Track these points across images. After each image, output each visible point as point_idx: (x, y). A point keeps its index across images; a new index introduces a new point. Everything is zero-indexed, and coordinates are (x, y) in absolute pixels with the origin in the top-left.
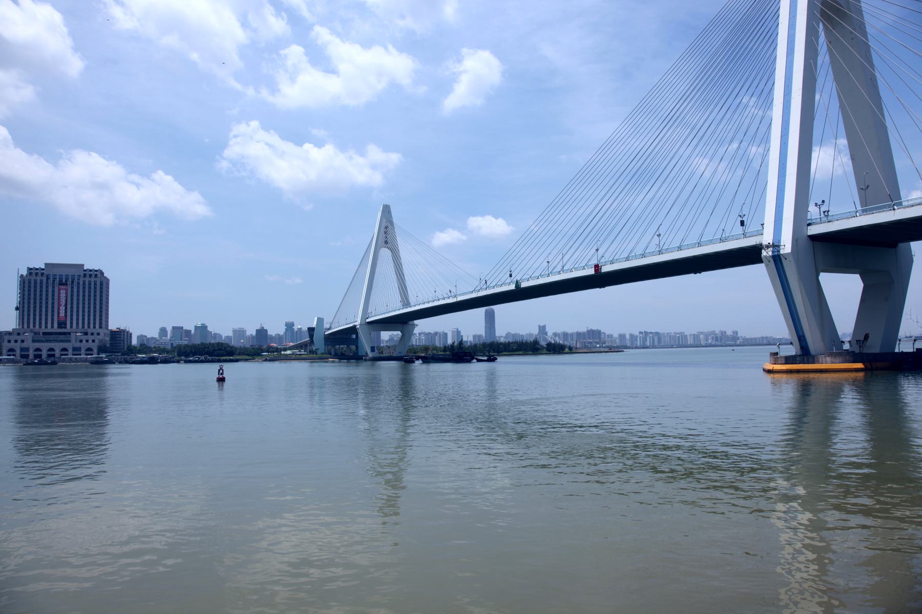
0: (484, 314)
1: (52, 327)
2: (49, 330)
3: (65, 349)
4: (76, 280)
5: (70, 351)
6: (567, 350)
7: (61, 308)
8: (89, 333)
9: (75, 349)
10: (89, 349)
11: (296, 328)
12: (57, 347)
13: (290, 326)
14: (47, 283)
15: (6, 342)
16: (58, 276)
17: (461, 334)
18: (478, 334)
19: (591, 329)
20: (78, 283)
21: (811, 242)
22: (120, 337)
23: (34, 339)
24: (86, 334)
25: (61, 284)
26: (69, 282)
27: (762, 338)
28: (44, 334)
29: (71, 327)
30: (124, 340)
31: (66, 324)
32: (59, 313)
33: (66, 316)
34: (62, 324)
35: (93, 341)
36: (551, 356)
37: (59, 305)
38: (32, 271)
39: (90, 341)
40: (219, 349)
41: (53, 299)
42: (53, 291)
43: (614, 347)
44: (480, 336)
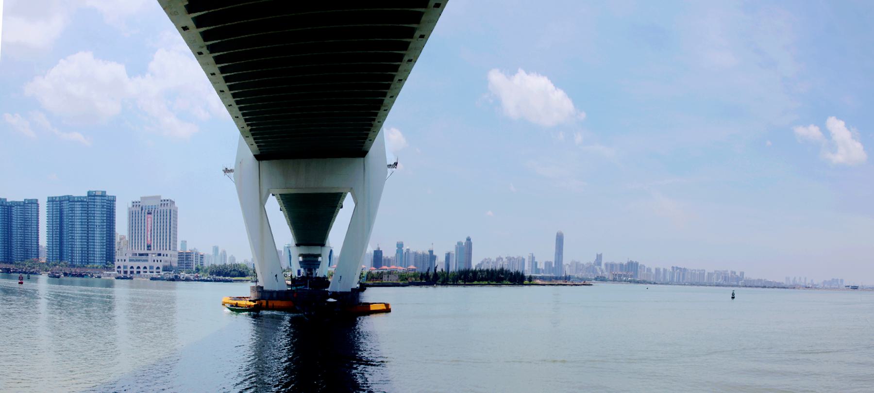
6: (526, 282)
11: (404, 249)
12: (142, 265)
14: (141, 213)
15: (117, 261)
17: (536, 261)
18: (549, 261)
21: (257, 162)
23: (131, 259)
24: (159, 255)
25: (149, 213)
26: (153, 212)
27: (759, 280)
34: (149, 247)
36: (455, 288)
37: (148, 231)
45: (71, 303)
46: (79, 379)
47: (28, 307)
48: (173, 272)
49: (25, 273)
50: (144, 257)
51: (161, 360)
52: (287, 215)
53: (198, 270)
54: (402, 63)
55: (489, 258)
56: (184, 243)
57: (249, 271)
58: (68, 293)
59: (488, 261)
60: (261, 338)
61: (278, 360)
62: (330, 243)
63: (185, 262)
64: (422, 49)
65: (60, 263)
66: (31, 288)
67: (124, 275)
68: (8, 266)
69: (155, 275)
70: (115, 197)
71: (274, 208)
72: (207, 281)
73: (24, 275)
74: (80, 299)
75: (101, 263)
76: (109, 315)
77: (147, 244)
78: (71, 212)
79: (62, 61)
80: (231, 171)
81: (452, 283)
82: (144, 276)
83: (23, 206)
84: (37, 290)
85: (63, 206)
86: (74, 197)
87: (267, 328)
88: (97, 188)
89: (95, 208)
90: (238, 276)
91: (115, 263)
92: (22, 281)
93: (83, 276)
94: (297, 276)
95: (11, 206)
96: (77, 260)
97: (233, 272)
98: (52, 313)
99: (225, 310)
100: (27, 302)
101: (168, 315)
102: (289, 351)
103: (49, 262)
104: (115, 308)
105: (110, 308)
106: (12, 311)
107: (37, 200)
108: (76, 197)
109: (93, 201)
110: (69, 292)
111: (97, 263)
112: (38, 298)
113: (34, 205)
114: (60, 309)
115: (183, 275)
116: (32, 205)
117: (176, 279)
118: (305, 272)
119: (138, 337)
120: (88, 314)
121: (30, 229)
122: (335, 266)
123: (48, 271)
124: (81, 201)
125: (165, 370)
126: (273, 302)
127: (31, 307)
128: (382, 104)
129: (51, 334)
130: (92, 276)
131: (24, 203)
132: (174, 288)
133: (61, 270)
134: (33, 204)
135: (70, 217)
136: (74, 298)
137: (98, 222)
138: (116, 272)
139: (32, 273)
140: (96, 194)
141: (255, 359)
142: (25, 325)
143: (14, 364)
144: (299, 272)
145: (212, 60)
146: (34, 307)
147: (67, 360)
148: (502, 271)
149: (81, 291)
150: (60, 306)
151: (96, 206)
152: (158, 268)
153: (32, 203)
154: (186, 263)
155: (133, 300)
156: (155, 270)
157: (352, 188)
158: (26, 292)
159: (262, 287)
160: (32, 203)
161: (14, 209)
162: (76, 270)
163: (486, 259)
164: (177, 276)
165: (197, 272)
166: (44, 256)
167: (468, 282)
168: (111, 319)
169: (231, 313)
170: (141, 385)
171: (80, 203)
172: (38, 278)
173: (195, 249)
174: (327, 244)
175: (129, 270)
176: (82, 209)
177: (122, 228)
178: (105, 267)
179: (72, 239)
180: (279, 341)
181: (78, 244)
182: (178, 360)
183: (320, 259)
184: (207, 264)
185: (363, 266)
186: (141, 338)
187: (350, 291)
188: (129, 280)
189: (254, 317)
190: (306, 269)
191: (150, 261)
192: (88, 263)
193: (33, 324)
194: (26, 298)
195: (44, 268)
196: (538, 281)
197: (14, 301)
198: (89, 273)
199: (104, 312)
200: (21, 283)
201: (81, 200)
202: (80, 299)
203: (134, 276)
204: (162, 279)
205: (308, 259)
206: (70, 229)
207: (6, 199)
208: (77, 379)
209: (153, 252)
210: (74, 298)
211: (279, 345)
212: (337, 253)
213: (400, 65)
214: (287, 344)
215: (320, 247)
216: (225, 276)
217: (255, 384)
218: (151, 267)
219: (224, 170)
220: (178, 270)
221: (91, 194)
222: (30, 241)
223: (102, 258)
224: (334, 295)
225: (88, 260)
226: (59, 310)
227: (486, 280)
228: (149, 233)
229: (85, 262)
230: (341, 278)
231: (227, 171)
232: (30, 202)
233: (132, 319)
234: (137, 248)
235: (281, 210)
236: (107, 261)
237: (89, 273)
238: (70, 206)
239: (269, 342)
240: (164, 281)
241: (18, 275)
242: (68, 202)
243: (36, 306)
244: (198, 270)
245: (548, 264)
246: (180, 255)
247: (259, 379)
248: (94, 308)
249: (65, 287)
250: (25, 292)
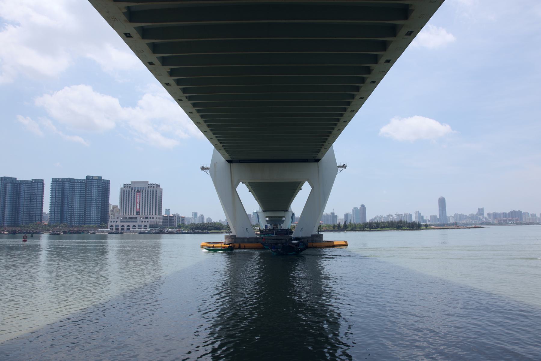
0: (438, 201)
1: (134, 214)
2: (132, 216)
3: (134, 226)
4: (145, 189)
5: (137, 227)
6: (422, 227)
7: (138, 204)
8: (149, 218)
9: (139, 226)
10: (145, 226)
12: (131, 224)
13: (195, 214)
14: (132, 191)
15: (110, 222)
16: (145, 188)
19: (514, 211)
20: (145, 191)
21: (229, 164)
24: (147, 218)
28: (130, 218)
29: (142, 214)
30: (175, 221)
31: (140, 213)
32: (136, 207)
33: (140, 209)
34: (138, 213)
35: (148, 222)
39: (146, 222)
40: (211, 226)
41: (134, 200)
42: (134, 196)
43: (448, 225)
45: (68, 252)
46: (73, 305)
47: (30, 258)
48: (158, 228)
49: (29, 233)
50: (133, 220)
51: (146, 285)
52: (255, 194)
54: (345, 112)
57: (224, 227)
58: (66, 245)
59: (381, 217)
60: (234, 266)
61: (250, 278)
62: (292, 209)
63: (169, 222)
65: (60, 225)
66: (34, 244)
67: (116, 231)
68: (14, 229)
70: (110, 180)
71: (243, 190)
73: (27, 235)
74: (76, 249)
76: (102, 258)
77: (136, 211)
78: (71, 189)
79: (66, 88)
80: (207, 168)
81: (359, 230)
83: (30, 184)
84: (39, 245)
85: (64, 185)
86: (75, 179)
87: (240, 260)
90: (214, 230)
91: (108, 223)
92: (26, 239)
93: (80, 233)
94: (264, 229)
95: (20, 184)
96: (76, 222)
97: (210, 227)
98: (52, 261)
99: (203, 250)
100: (28, 255)
101: (153, 255)
102: (259, 273)
103: (51, 224)
104: (107, 253)
105: (103, 253)
106: (14, 263)
107: (43, 180)
108: (76, 179)
110: (67, 244)
112: (39, 251)
113: (40, 183)
114: (58, 257)
116: (38, 183)
119: (126, 271)
120: (83, 259)
121: (36, 201)
122: (297, 222)
123: (50, 231)
124: (81, 183)
125: (151, 291)
127: (33, 257)
128: (331, 133)
129: (49, 276)
130: (88, 232)
131: (32, 181)
132: (159, 239)
133: (61, 230)
134: (40, 183)
135: (70, 193)
136: (71, 249)
137: (94, 196)
139: (36, 233)
140: (93, 178)
141: (230, 278)
142: (26, 272)
143: (13, 303)
144: (266, 227)
145: (191, 105)
146: (35, 257)
147: (62, 293)
148: (401, 222)
149: (78, 243)
150: (59, 255)
151: (93, 186)
153: (38, 182)
154: (169, 223)
155: (123, 247)
158: (29, 247)
159: (236, 236)
160: (38, 182)
161: (23, 186)
162: (74, 229)
165: (179, 228)
166: (47, 220)
167: (372, 229)
168: (103, 261)
169: (208, 252)
170: (128, 303)
171: (79, 184)
172: (40, 236)
173: (177, 214)
174: (289, 210)
175: (120, 228)
176: (81, 188)
177: (115, 199)
178: (99, 226)
179: (71, 208)
180: (251, 267)
181: (76, 211)
182: (162, 283)
185: (321, 222)
186: (129, 272)
187: (311, 236)
189: (228, 254)
190: (272, 225)
191: (138, 222)
192: (85, 224)
193: (33, 271)
194: (28, 252)
195: (46, 229)
197: (18, 255)
198: (86, 231)
199: (97, 257)
200: (25, 241)
201: (80, 181)
202: (76, 249)
203: (125, 231)
204: (149, 233)
205: (273, 219)
206: (70, 201)
207: (16, 178)
208: (70, 305)
209: (141, 216)
210: (71, 249)
211: (250, 269)
213: (345, 113)
214: (257, 268)
215: (283, 212)
216: (203, 230)
217: (230, 294)
218: (139, 226)
220: (164, 226)
221: (89, 178)
222: (35, 211)
224: (297, 239)
225: (85, 222)
226: (58, 258)
227: (388, 228)
229: (82, 223)
231: (203, 168)
232: (36, 181)
233: (123, 260)
235: (249, 191)
237: (86, 231)
238: (71, 185)
239: (241, 268)
240: (151, 234)
241: (23, 235)
242: (69, 182)
243: (37, 257)
244: (179, 227)
246: (165, 218)
247: (234, 291)
248: (89, 254)
249: (64, 241)
250: (28, 248)
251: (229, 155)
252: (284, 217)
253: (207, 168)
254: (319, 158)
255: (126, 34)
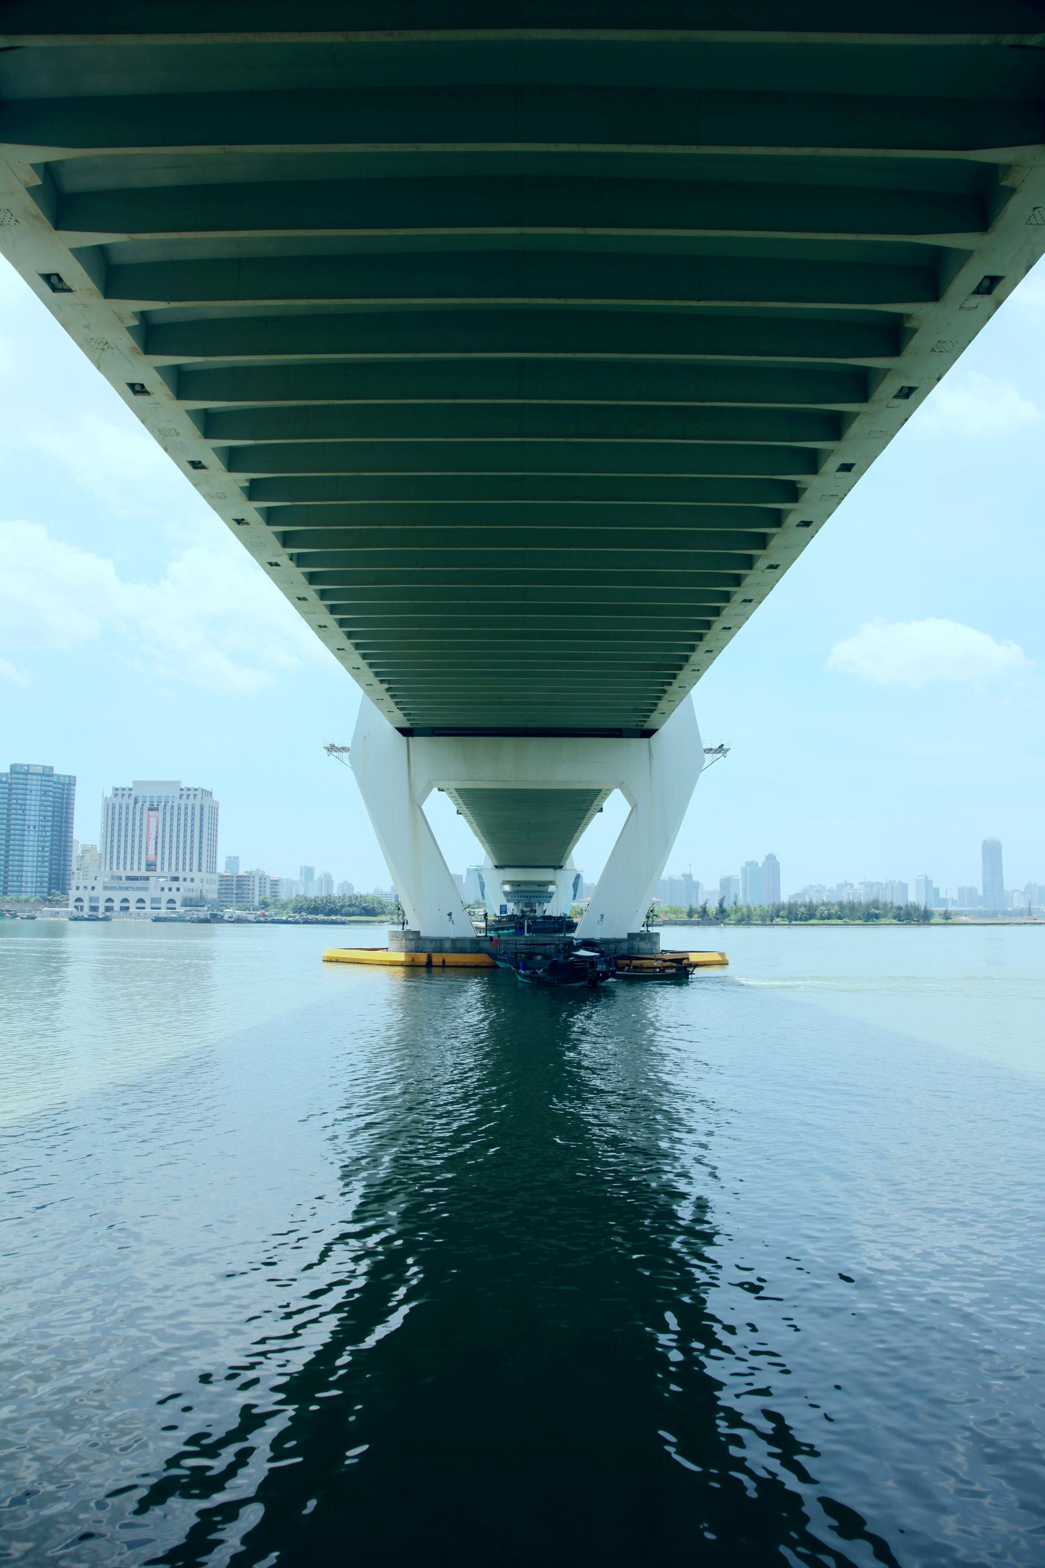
1: (139, 869)
3: (141, 901)
9: (153, 900)
13: (308, 872)
14: (134, 808)
15: (74, 888)
16: (156, 798)
20: (172, 807)
22: (249, 885)
24: (176, 879)
25: (151, 809)
26: (161, 807)
28: (129, 878)
29: (162, 869)
34: (151, 866)
35: (178, 889)
37: (148, 839)
38: (125, 792)
39: (174, 890)
40: (350, 906)
43: (1006, 913)
44: (972, 891)
53: (265, 905)
55: (820, 885)
56: (233, 861)
63: (235, 892)
64: (774, 585)
69: (163, 912)
72: (286, 922)
75: (36, 892)
81: (759, 922)
82: (139, 914)
88: (34, 757)
89: (26, 795)
90: (361, 915)
91: (70, 892)
109: (25, 781)
111: (26, 892)
115: (228, 912)
117: (215, 919)
118: (518, 909)
126: (444, 955)
137: (33, 817)
138: (71, 909)
152: (171, 901)
154: (236, 894)
156: (164, 904)
157: (623, 783)
159: (418, 933)
163: (811, 886)
164: (216, 915)
165: (262, 908)
174: (568, 865)
175: (102, 905)
183: (551, 888)
184: (283, 896)
188: (103, 923)
190: (521, 904)
196: (963, 919)
204: (180, 919)
205: (523, 888)
212: (591, 877)
216: (329, 914)
219: (326, 748)
220: (222, 904)
223: (39, 884)
224: (588, 944)
228: (152, 843)
230: (602, 918)
234: (188, 868)
236: (50, 889)
240: (187, 923)
244: (265, 905)
245: (966, 893)
246: (225, 882)
251: (405, 715)
252: (552, 883)
253: (342, 748)
254: (656, 727)
255: (132, 386)
